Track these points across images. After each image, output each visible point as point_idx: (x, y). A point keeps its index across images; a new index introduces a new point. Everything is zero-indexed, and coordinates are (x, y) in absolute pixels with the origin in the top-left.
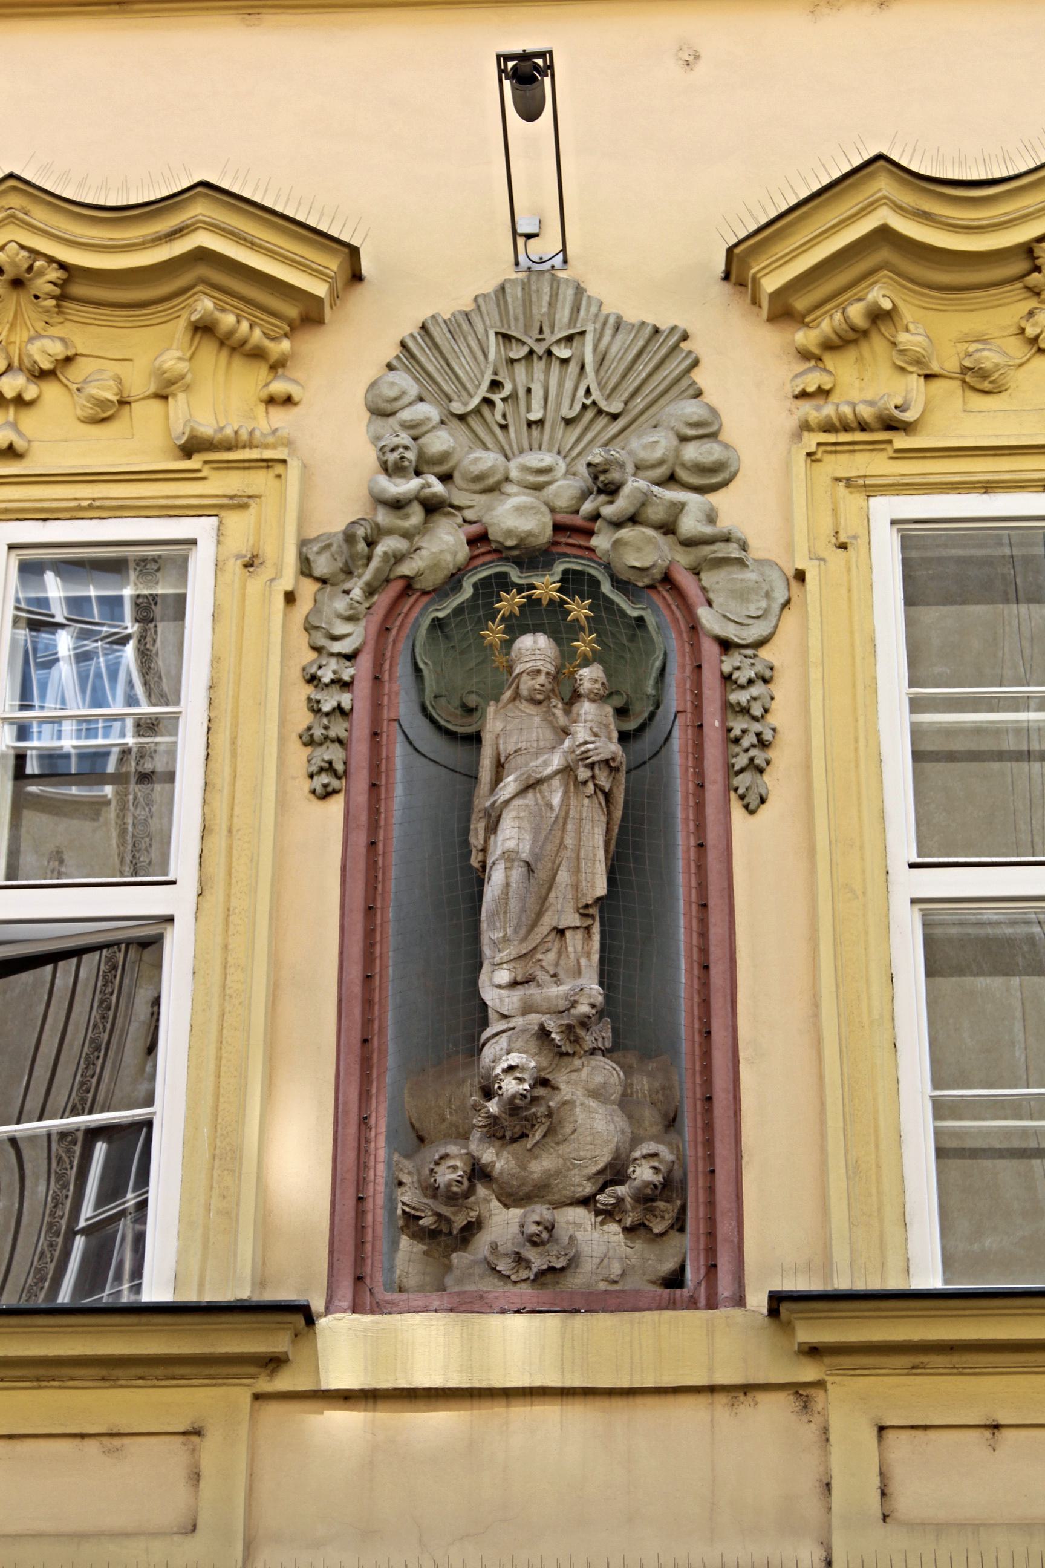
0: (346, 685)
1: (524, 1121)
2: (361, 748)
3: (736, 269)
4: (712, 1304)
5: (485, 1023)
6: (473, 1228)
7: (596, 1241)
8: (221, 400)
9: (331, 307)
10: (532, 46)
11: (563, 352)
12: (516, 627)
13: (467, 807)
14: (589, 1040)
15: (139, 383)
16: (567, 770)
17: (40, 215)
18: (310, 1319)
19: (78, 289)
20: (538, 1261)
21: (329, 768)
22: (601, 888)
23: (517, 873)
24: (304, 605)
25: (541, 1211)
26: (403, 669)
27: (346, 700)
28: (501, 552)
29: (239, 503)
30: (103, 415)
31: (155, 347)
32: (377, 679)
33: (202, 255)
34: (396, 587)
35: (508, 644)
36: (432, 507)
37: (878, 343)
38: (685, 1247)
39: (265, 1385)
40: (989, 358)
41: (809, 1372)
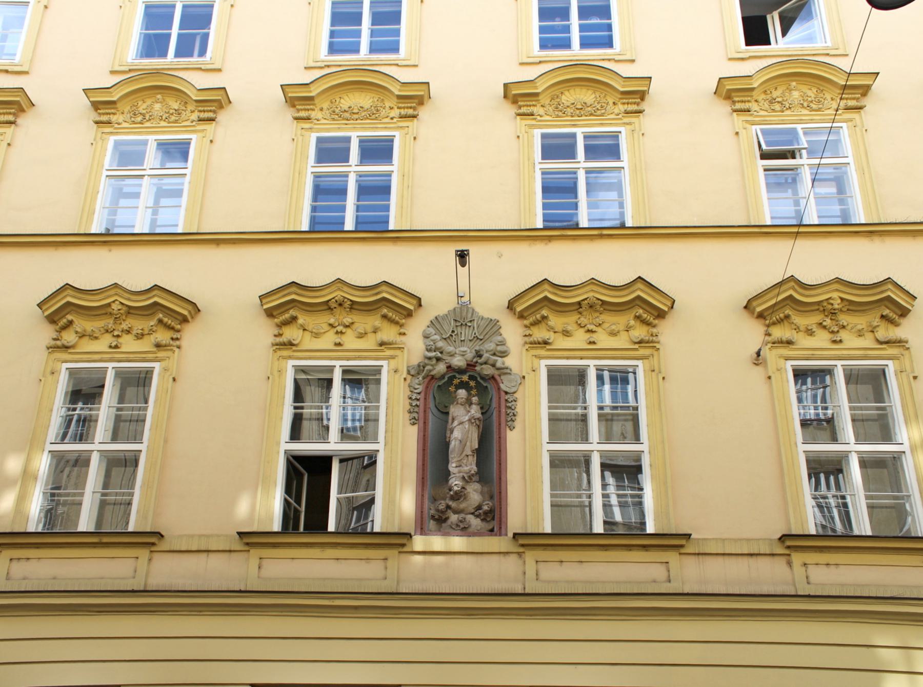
0: (418, 400)
1: (458, 496)
2: (422, 414)
3: (511, 306)
4: (500, 535)
5: (449, 475)
6: (447, 519)
7: (475, 522)
8: (388, 333)
9: (906, 423)
10: (464, 248)
11: (469, 324)
12: (458, 387)
13: (446, 427)
14: (474, 479)
15: (369, 328)
16: (469, 420)
17: (345, 289)
18: (411, 537)
19: (355, 307)
20: (462, 526)
21: (414, 418)
22: (477, 447)
23: (457, 442)
24: (408, 381)
25: (462, 515)
26: (431, 396)
27: (418, 403)
28: (454, 370)
29: (393, 357)
30: (361, 336)
31: (374, 320)
32: (425, 399)
33: (384, 299)
34: (429, 378)
35: (455, 392)
36: (438, 359)
37: (543, 324)
38: (495, 524)
39: (401, 550)
40: (569, 328)
41: (521, 550)
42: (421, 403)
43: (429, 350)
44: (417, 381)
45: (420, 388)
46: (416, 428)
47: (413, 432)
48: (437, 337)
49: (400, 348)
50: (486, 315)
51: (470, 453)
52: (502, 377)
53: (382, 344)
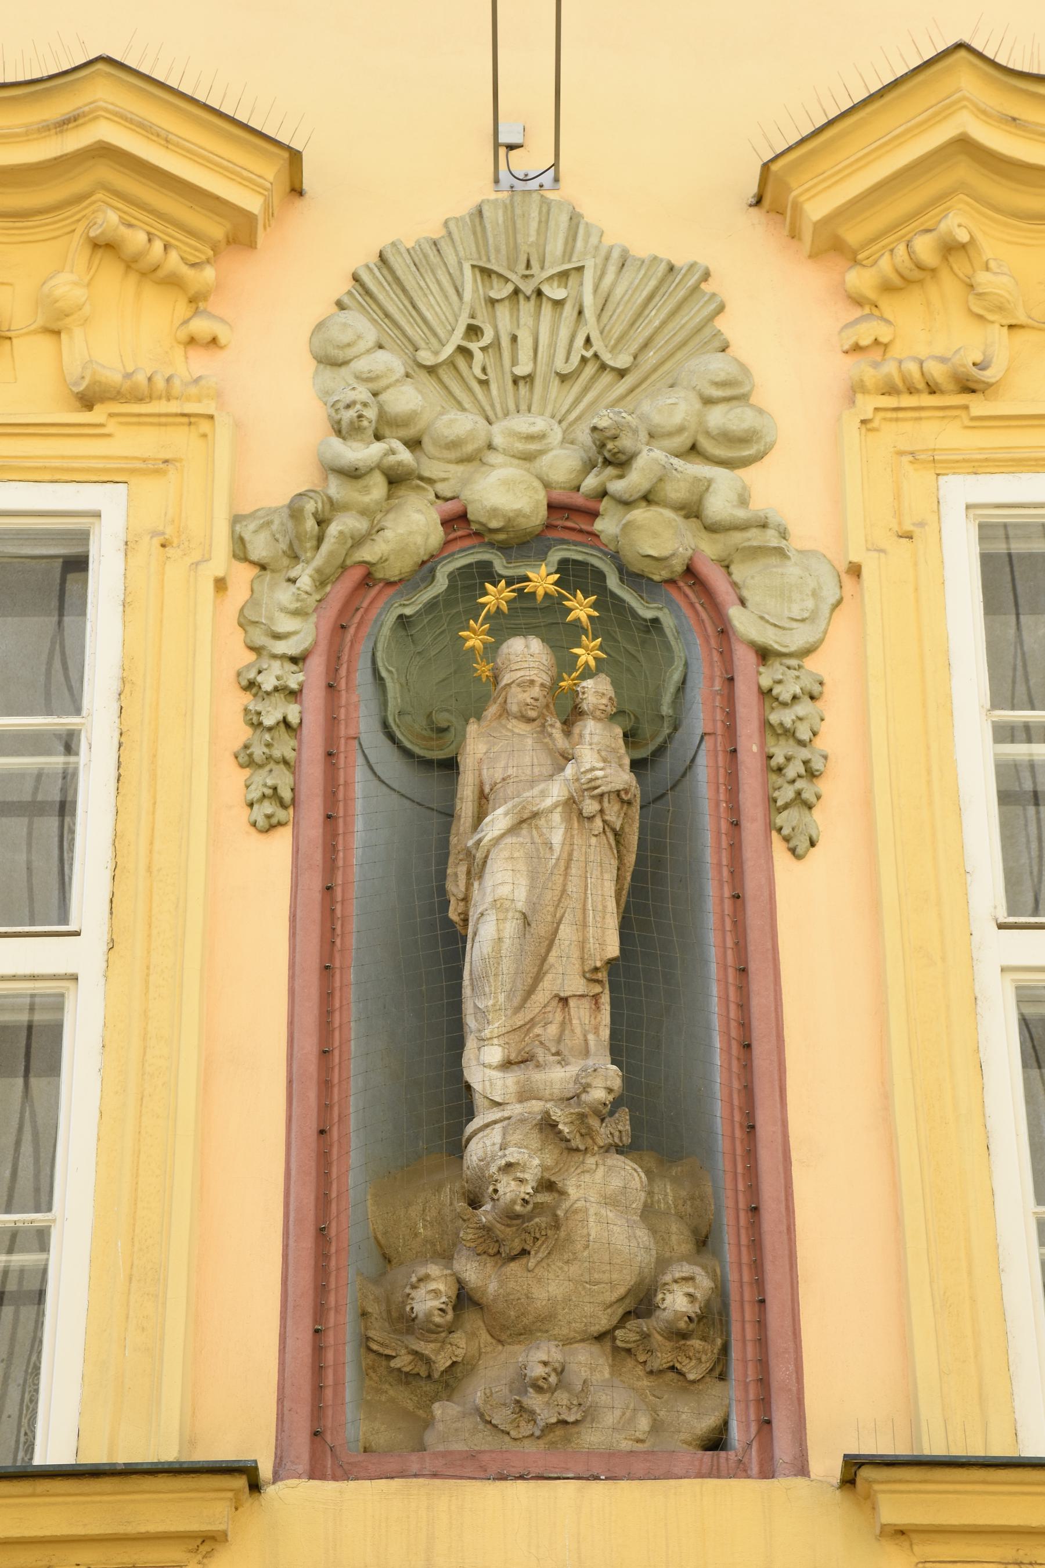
0: (294, 695)
2: (313, 771)
4: (767, 1472)
5: (470, 1114)
8: (126, 333)
12: (504, 626)
13: (444, 844)
16: (571, 805)
22: (613, 950)
23: (511, 927)
24: (238, 595)
26: (362, 676)
28: (481, 535)
33: (104, 152)
35: (491, 651)
36: (396, 480)
38: (733, 1403)
42: (309, 714)
44: (285, 595)
45: (302, 634)
47: (267, 871)
49: (189, 418)
50: (648, 241)
51: (575, 985)
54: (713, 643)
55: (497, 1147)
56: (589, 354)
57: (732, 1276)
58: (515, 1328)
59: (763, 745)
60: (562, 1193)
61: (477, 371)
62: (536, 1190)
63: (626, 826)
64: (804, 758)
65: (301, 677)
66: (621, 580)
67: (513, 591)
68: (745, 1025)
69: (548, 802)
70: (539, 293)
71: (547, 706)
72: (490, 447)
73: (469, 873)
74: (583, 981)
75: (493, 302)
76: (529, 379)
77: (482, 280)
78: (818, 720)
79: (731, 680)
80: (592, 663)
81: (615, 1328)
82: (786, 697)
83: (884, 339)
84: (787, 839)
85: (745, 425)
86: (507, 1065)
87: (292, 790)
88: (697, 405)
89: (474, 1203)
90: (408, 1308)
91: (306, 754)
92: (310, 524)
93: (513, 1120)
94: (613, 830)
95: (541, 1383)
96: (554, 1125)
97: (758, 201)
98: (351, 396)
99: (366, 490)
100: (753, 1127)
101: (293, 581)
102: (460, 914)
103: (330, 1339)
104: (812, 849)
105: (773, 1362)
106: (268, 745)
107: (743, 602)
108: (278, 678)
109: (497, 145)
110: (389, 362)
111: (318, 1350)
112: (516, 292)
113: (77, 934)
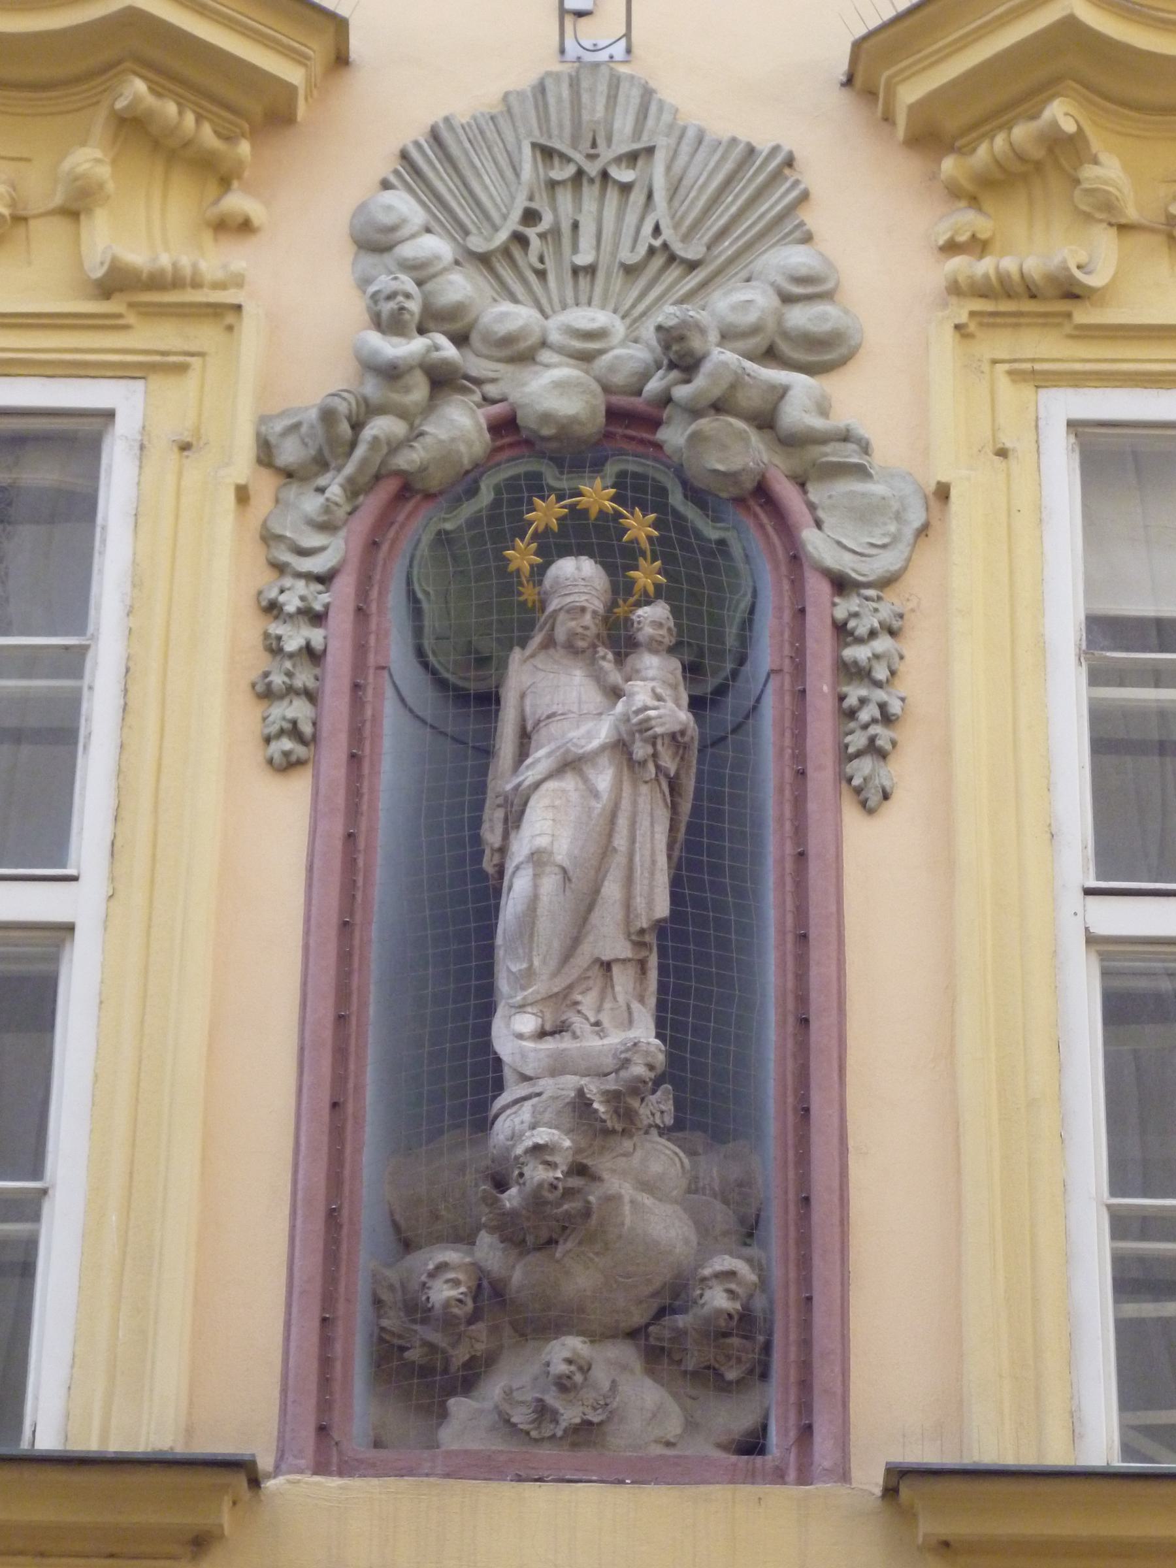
0: (317, 618)
1: (555, 1222)
2: (336, 703)
3: (868, 69)
4: (805, 1477)
8: (142, 227)
11: (624, 175)
12: (552, 547)
13: (481, 789)
15: (41, 191)
16: (621, 747)
18: (255, 1482)
20: (571, 1415)
21: (293, 731)
22: (662, 908)
23: (550, 883)
27: (316, 636)
29: (171, 367)
32: (361, 612)
34: (389, 487)
35: (539, 572)
36: (443, 381)
42: (335, 638)
43: (392, 325)
44: (311, 504)
46: (297, 792)
47: (282, 821)
48: (436, 246)
51: (616, 946)
52: (816, 493)
53: (116, 283)
54: (784, 570)
55: (526, 1125)
56: (657, 243)
57: (777, 1273)
58: (540, 1322)
59: (836, 684)
60: (595, 1178)
61: (533, 259)
62: (568, 1174)
63: (683, 772)
64: (879, 700)
65: (325, 598)
66: (686, 496)
67: (562, 507)
68: (802, 999)
69: (595, 744)
70: (605, 175)
71: (598, 636)
72: (544, 344)
73: (506, 820)
74: (628, 945)
75: (553, 185)
76: (591, 270)
77: (543, 160)
78: (897, 658)
79: (802, 611)
80: (651, 590)
81: (647, 1325)
82: (862, 631)
83: (982, 236)
84: (858, 791)
85: (827, 327)
86: (542, 1034)
87: (314, 724)
88: (775, 301)
89: (501, 1185)
90: (424, 1298)
91: (330, 685)
92: (345, 428)
93: (544, 1097)
94: (667, 776)
95: (565, 1381)
96: (588, 1104)
97: (849, 81)
98: (395, 286)
99: (407, 390)
100: (807, 1110)
101: (321, 490)
102: (495, 866)
103: (340, 1330)
104: (886, 803)
105: (817, 1362)
106: (289, 674)
107: (819, 524)
108: (302, 598)
109: (563, 12)
110: (436, 246)
111: (326, 1341)
112: (580, 173)
113: (74, 879)
